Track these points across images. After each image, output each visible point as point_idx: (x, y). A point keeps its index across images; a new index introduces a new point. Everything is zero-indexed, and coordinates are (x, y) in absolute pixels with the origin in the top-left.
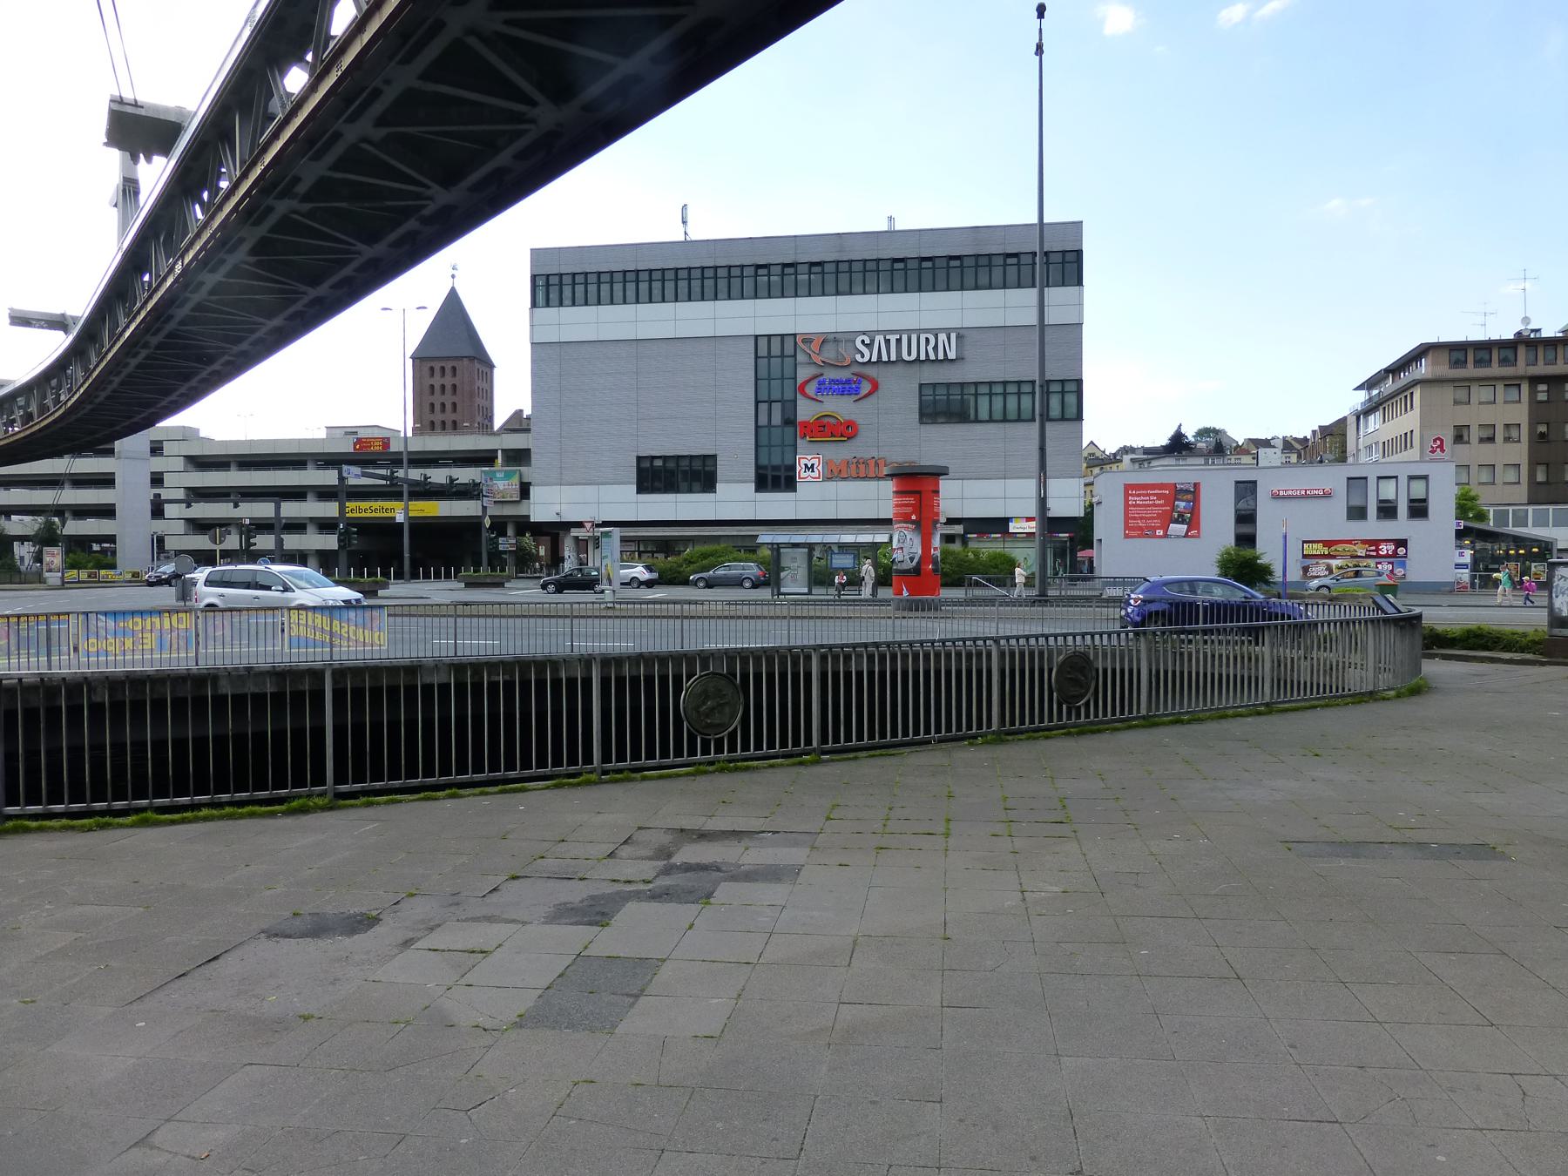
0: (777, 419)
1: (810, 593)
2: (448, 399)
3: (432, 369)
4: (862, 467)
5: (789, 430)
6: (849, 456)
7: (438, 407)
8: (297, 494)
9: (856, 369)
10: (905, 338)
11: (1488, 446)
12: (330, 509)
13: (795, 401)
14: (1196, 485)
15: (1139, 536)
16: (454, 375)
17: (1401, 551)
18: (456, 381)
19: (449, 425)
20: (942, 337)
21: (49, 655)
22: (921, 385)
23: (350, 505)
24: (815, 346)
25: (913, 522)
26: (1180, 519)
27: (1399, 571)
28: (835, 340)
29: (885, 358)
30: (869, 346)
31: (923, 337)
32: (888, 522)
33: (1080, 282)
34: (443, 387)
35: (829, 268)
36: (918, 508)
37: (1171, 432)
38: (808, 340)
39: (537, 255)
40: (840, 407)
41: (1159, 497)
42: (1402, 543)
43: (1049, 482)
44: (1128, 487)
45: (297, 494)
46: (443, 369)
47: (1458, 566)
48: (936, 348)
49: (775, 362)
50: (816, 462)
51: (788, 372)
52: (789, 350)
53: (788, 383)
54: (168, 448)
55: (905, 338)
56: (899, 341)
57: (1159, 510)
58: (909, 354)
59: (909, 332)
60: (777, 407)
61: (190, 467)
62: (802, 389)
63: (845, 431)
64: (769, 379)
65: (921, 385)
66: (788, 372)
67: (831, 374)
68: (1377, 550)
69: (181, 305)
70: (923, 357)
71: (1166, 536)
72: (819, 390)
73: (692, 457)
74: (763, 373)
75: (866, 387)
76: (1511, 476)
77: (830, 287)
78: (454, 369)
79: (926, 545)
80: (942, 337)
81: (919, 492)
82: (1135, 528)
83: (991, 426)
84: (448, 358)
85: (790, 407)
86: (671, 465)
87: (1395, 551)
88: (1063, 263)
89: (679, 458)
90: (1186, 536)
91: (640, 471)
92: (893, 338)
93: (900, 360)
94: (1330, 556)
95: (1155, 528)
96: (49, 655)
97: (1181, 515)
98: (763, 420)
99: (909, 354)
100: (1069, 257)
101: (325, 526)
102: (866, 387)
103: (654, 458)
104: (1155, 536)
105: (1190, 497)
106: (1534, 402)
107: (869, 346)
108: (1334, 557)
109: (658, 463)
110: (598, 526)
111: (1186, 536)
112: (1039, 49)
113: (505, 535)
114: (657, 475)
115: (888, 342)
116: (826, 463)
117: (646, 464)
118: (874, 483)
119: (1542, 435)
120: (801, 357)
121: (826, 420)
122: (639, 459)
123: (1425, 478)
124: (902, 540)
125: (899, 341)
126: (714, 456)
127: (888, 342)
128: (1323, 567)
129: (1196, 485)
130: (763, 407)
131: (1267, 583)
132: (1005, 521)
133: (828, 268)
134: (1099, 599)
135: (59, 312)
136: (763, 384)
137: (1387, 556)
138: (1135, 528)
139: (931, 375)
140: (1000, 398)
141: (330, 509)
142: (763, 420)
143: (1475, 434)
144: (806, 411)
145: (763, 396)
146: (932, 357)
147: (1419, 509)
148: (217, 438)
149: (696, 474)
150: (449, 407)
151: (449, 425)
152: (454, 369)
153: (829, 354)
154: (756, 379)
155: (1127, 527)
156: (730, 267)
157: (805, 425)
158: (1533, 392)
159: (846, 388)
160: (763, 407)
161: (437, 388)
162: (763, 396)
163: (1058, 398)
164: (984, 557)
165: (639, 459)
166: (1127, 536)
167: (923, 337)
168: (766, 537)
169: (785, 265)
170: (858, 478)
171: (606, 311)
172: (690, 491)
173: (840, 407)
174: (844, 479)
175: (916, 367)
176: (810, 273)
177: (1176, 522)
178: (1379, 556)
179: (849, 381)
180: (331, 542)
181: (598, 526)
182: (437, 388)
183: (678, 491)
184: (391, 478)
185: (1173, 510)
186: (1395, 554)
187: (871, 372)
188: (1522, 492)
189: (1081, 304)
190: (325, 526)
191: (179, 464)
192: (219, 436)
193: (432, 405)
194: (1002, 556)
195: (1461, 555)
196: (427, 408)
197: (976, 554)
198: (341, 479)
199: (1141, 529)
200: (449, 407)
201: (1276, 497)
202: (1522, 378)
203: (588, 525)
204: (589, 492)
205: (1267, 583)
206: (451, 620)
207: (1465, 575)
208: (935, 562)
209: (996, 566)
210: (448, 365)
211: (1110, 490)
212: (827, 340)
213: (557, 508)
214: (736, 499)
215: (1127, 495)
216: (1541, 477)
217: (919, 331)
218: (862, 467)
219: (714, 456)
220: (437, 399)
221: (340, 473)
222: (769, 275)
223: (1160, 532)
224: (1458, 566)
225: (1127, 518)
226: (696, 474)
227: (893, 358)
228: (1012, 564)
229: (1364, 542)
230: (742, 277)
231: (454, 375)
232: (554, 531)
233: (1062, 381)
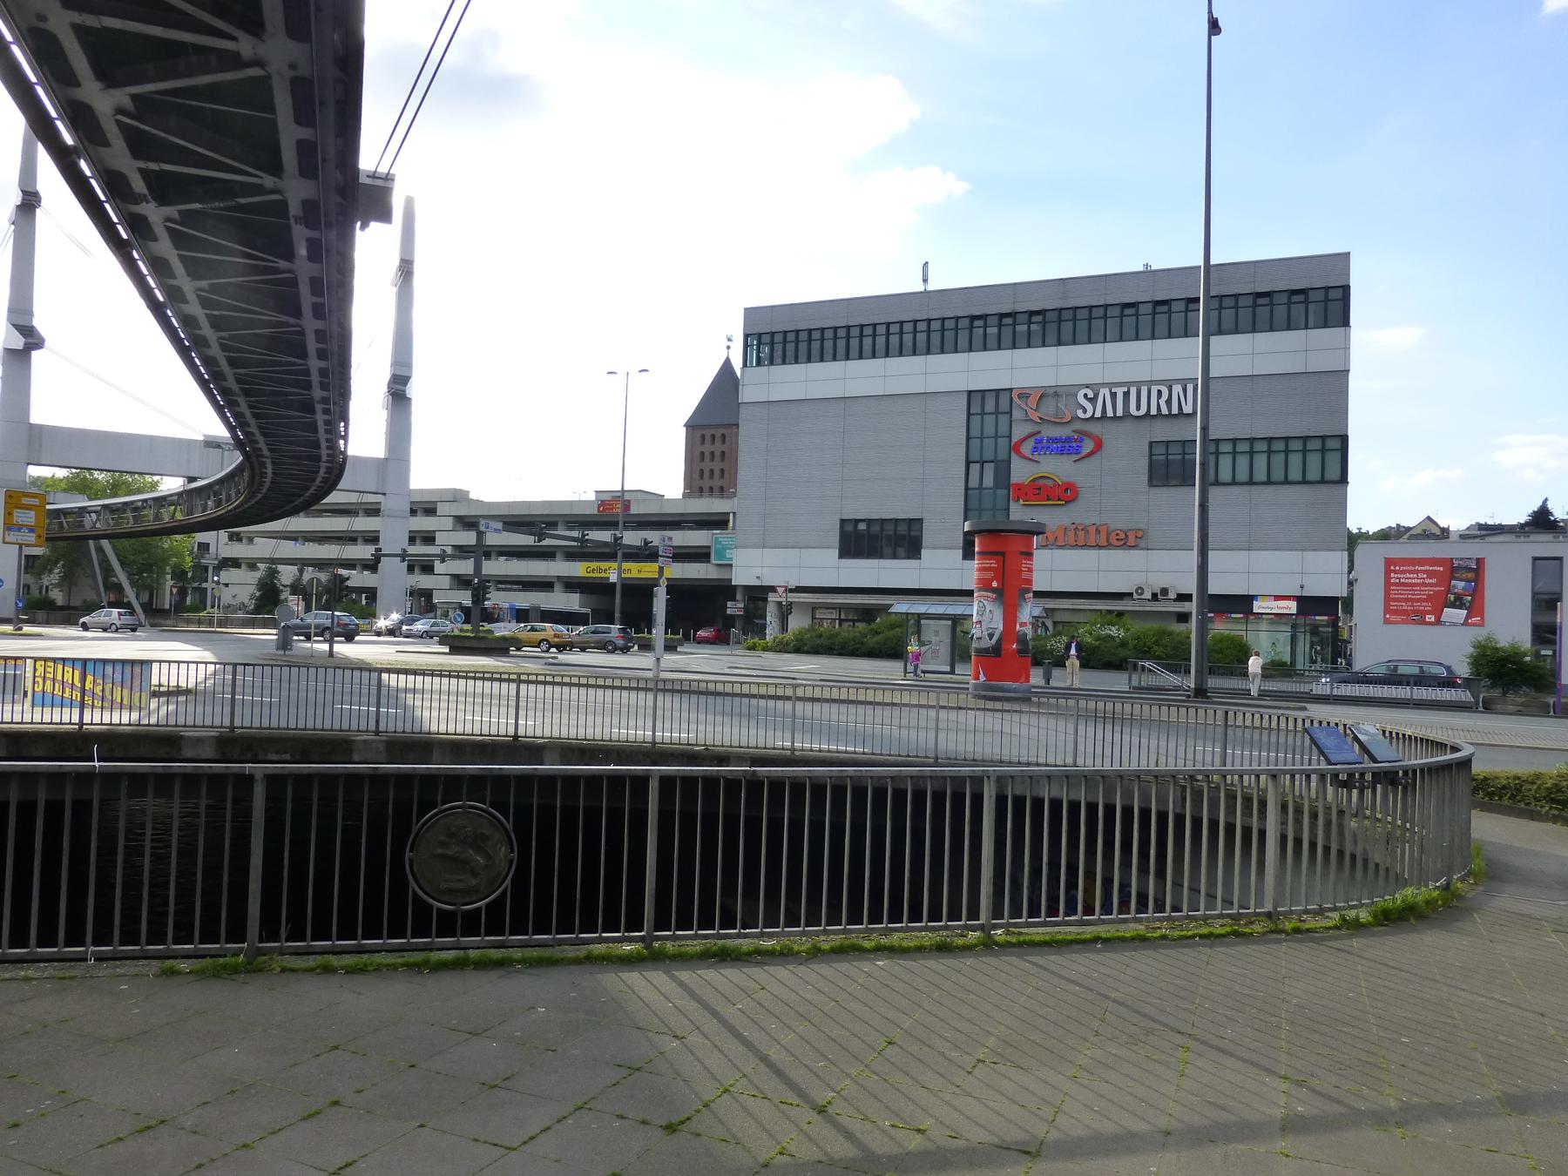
0: (989, 481)
1: (952, 672)
3: (703, 437)
5: (1002, 492)
6: (1067, 522)
7: (707, 473)
8: (544, 585)
9: (1077, 426)
10: (1133, 391)
12: (579, 569)
13: (1009, 461)
14: (1480, 562)
15: (1403, 622)
16: (724, 442)
18: (725, 448)
19: (706, 489)
20: (1177, 389)
21: (233, 700)
22: (1151, 443)
23: (625, 565)
24: (1032, 402)
25: (993, 590)
26: (1458, 603)
28: (1056, 395)
29: (1110, 413)
30: (1093, 400)
31: (1154, 390)
32: (969, 593)
33: (1345, 322)
34: (712, 454)
35: (1052, 316)
36: (1002, 573)
37: (1535, 506)
38: (1024, 396)
39: (750, 313)
40: (1057, 468)
41: (1431, 574)
44: (1389, 562)
45: (544, 585)
46: (713, 436)
48: (1169, 402)
49: (990, 420)
51: (1003, 429)
52: (1004, 406)
53: (1003, 442)
54: (441, 509)
55: (1133, 391)
56: (1126, 394)
57: (1430, 591)
58: (1138, 408)
59: (1139, 384)
60: (989, 468)
61: (459, 527)
62: (1016, 448)
63: (1065, 494)
64: (982, 438)
65: (1151, 443)
66: (1003, 429)
67: (1049, 432)
70: (1154, 411)
71: (1438, 622)
72: (1035, 449)
73: (883, 521)
74: (975, 432)
75: (1088, 446)
77: (1051, 337)
78: (724, 436)
79: (1010, 617)
80: (1177, 389)
81: (1003, 554)
82: (1399, 610)
83: (1235, 490)
84: (718, 426)
85: (1003, 469)
86: (876, 528)
88: (1327, 300)
89: (883, 521)
90: (1465, 623)
91: (844, 536)
92: (1120, 392)
93: (1127, 415)
95: (1425, 613)
96: (233, 700)
97: (1459, 597)
98: (974, 482)
99: (1138, 408)
100: (1333, 294)
101: (571, 585)
102: (1088, 446)
103: (857, 521)
104: (1425, 623)
105: (1470, 575)
107: (1093, 400)
109: (862, 526)
110: (791, 591)
111: (1465, 623)
112: (1214, 27)
113: (734, 599)
114: (860, 540)
115: (1114, 395)
117: (849, 528)
118: (1093, 553)
120: (1017, 414)
121: (1042, 482)
122: (843, 522)
124: (981, 613)
125: (1126, 394)
126: (920, 521)
127: (1114, 395)
129: (1480, 562)
133: (1050, 316)
136: (975, 443)
138: (1399, 610)
139: (1163, 431)
140: (1264, 457)
141: (579, 569)
142: (974, 482)
144: (1021, 472)
145: (975, 456)
146: (1165, 411)
148: (487, 499)
149: (903, 539)
150: (717, 473)
151: (706, 489)
152: (724, 436)
153: (1048, 409)
154: (968, 438)
155: (1387, 610)
156: (944, 319)
157: (1019, 487)
159: (1066, 446)
160: (975, 468)
163: (1322, 457)
165: (843, 522)
166: (1386, 621)
167: (1154, 390)
168: (901, 606)
169: (1002, 316)
171: (816, 369)
172: (895, 556)
173: (1057, 468)
174: (1061, 547)
175: (1146, 423)
176: (1030, 323)
177: (1453, 605)
179: (1069, 440)
181: (791, 591)
183: (881, 557)
184: (541, 537)
185: (1448, 591)
187: (1095, 429)
189: (1347, 348)
190: (571, 585)
191: (448, 523)
192: (487, 498)
193: (702, 471)
194: (1230, 639)
196: (696, 475)
199: (1405, 612)
200: (717, 473)
203: (780, 590)
204: (791, 555)
206: (513, 686)
208: (1022, 639)
209: (1220, 651)
210: (708, 433)
211: (1370, 562)
212: (1044, 395)
213: (758, 572)
215: (1388, 572)
217: (1150, 383)
219: (920, 521)
220: (707, 465)
222: (985, 326)
223: (1431, 618)
225: (1388, 599)
226: (903, 539)
227: (1120, 413)
228: (1244, 653)
230: (957, 329)
231: (724, 442)
232: (757, 595)
233: (1323, 438)
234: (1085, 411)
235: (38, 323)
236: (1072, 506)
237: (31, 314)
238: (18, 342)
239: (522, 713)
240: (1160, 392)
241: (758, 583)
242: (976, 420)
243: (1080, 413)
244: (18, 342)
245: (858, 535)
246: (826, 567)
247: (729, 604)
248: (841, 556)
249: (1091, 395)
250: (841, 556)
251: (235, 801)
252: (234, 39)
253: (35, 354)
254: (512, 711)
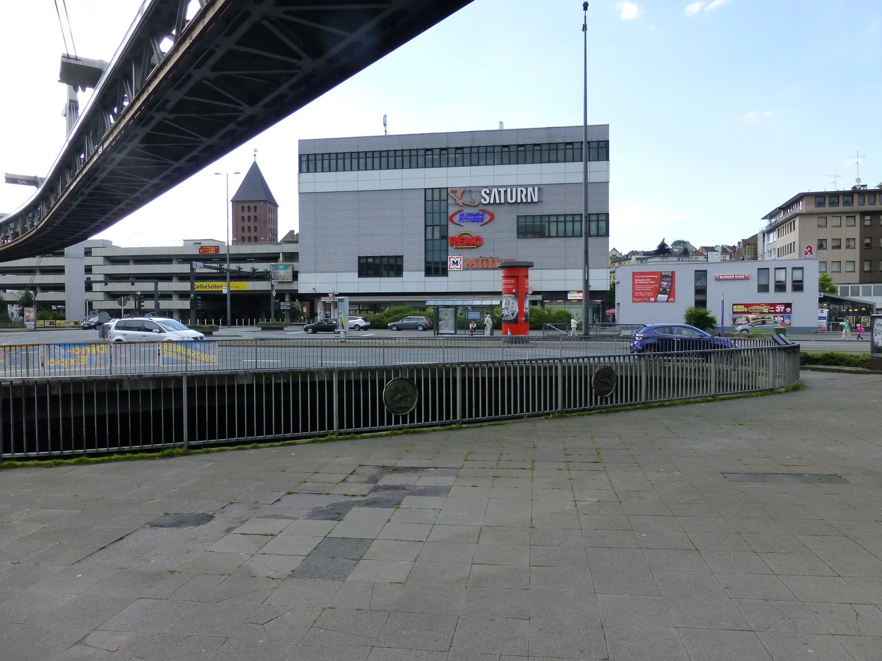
0: (437, 235)
1: (455, 333)
2: (252, 224)
3: (243, 207)
4: (485, 262)
5: (444, 242)
6: (478, 257)
7: (246, 229)
8: (167, 277)
9: (481, 207)
10: (509, 190)
11: (837, 251)
12: (185, 286)
13: (447, 225)
14: (673, 273)
15: (641, 302)
16: (256, 211)
17: (788, 310)
18: (257, 214)
19: (253, 239)
20: (530, 189)
21: (28, 368)
22: (518, 217)
23: (197, 284)
24: (458, 195)
25: (513, 293)
26: (664, 292)
27: (787, 321)
28: (470, 191)
29: (498, 201)
30: (489, 194)
31: (519, 190)
32: (499, 293)
33: (607, 159)
34: (249, 217)
35: (466, 151)
36: (517, 286)
37: (659, 243)
38: (454, 191)
39: (302, 143)
40: (472, 229)
41: (652, 279)
42: (789, 305)
43: (590, 271)
44: (634, 274)
45: (167, 277)
46: (249, 207)
47: (820, 318)
48: (526, 195)
49: (436, 203)
50: (459, 259)
51: (443, 209)
52: (444, 197)
53: (443, 216)
54: (94, 252)
55: (509, 190)
56: (506, 192)
57: (652, 287)
58: (512, 199)
59: (511, 186)
60: (437, 229)
61: (107, 263)
62: (451, 218)
63: (475, 242)
64: (433, 213)
65: (518, 217)
66: (443, 209)
67: (467, 210)
68: (775, 309)
69: (102, 172)
70: (519, 201)
71: (656, 301)
72: (461, 219)
73: (389, 257)
74: (429, 210)
75: (487, 218)
76: (850, 267)
77: (467, 161)
78: (255, 207)
79: (521, 306)
80: (530, 189)
81: (517, 277)
82: (638, 297)
83: (558, 239)
84: (252, 201)
85: (444, 229)
86: (377, 261)
87: (785, 310)
88: (598, 148)
89: (382, 257)
90: (667, 301)
91: (360, 265)
92: (502, 190)
93: (506, 202)
94: (748, 313)
95: (650, 297)
96: (28, 368)
97: (664, 289)
98: (429, 236)
99: (512, 199)
100: (601, 145)
101: (183, 295)
102: (487, 218)
103: (368, 257)
104: (650, 301)
105: (669, 279)
106: (863, 226)
107: (489, 194)
108: (750, 313)
109: (370, 260)
110: (337, 295)
111: (667, 301)
113: (284, 301)
114: (369, 267)
115: (499, 192)
116: (465, 260)
117: (364, 261)
118: (491, 272)
119: (867, 245)
120: (450, 201)
121: (464, 236)
122: (360, 258)
123: (802, 268)
124: (507, 304)
125: (506, 192)
126: (402, 257)
127: (499, 192)
128: (744, 319)
129: (673, 273)
130: (429, 229)
131: (713, 327)
132: (565, 293)
133: (466, 151)
134: (618, 336)
135: (33, 175)
136: (429, 216)
137: (780, 312)
138: (638, 297)
139: (523, 211)
140: (563, 224)
141: (185, 286)
142: (429, 236)
143: (830, 244)
144: (453, 231)
145: (429, 222)
146: (524, 200)
147: (798, 286)
148: (122, 246)
149: (392, 266)
150: (252, 229)
151: (253, 239)
152: (255, 207)
153: (466, 199)
154: (426, 213)
155: (634, 296)
156: (411, 150)
157: (453, 239)
158: (862, 221)
159: (476, 218)
160: (429, 229)
161: (246, 218)
162: (429, 222)
163: (595, 224)
164: (553, 313)
165: (360, 258)
166: (634, 301)
167: (519, 190)
168: (431, 302)
169: (441, 149)
170: (483, 269)
171: (341, 175)
172: (388, 276)
173: (472, 229)
174: (475, 269)
175: (515, 206)
176: (456, 154)
177: (662, 293)
178: (776, 313)
179: (477, 214)
180: (186, 305)
181: (337, 295)
182: (246, 218)
183: (381, 276)
184: (220, 269)
185: (660, 286)
186: (785, 312)
187: (490, 209)
188: (856, 276)
189: (608, 171)
190: (183, 295)
191: (101, 261)
192: (123, 245)
193: (243, 228)
194: (563, 312)
195: (822, 312)
196: (240, 230)
197: (549, 312)
198: (192, 269)
199: (642, 297)
200: (252, 229)
201: (718, 279)
202: (856, 212)
203: (331, 295)
204: (332, 276)
205: (713, 327)
206: (254, 349)
207: (824, 323)
208: (526, 316)
209: (560, 318)
210: (252, 205)
211: (624, 275)
212: (465, 191)
213: (313, 286)
214: (414, 280)
215: (634, 278)
216: (867, 268)
217: (517, 186)
218: (485, 262)
219: (402, 257)
220: (246, 224)
221: (191, 266)
222: (433, 155)
223: (652, 299)
224: (820, 318)
225: (634, 291)
226: (392, 266)
227: (502, 201)
228: (569, 317)
229: (767, 305)
230: (417, 155)
231: (256, 211)
232: (311, 299)
233: (598, 214)
239: (31, 365)
251: (27, 423)
252: (285, 13)
254: (24, 365)
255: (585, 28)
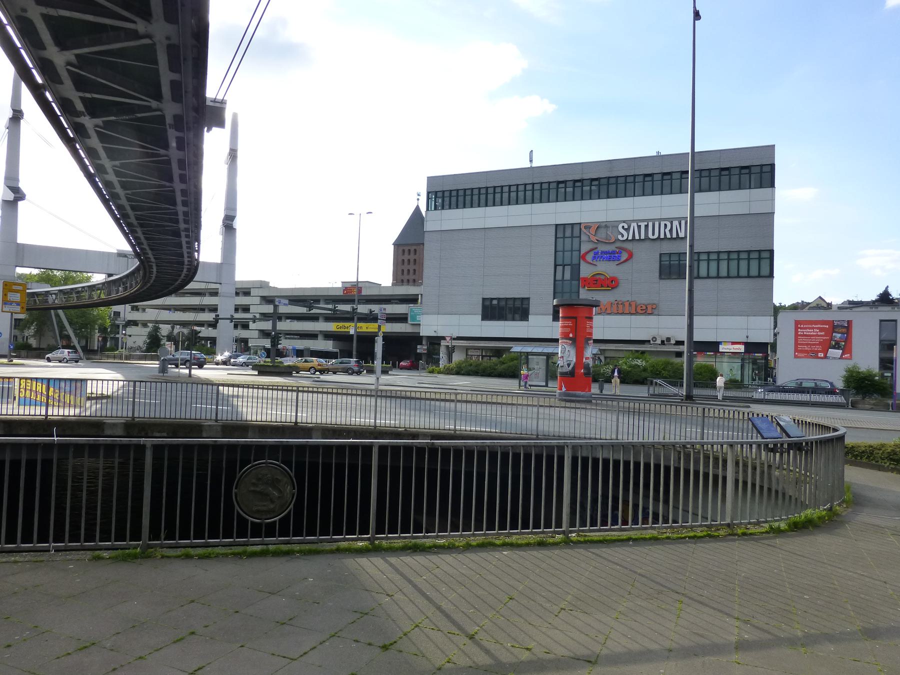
0: (567, 276)
1: (547, 386)
3: (404, 251)
5: (575, 283)
6: (612, 300)
7: (406, 272)
9: (618, 244)
10: (650, 225)
12: (332, 327)
13: (579, 264)
14: (850, 322)
15: (805, 357)
16: (415, 254)
18: (416, 257)
19: (405, 281)
20: (676, 223)
21: (134, 402)
22: (661, 254)
23: (359, 325)
24: (593, 231)
25: (570, 339)
26: (837, 346)
28: (606, 227)
29: (637, 237)
30: (627, 230)
31: (662, 224)
32: (556, 341)
33: (772, 185)
34: (409, 260)
35: (604, 182)
36: (575, 329)
37: (881, 290)
38: (588, 227)
39: (431, 180)
40: (607, 268)
41: (821, 330)
44: (797, 323)
46: (409, 250)
48: (671, 231)
49: (568, 241)
51: (576, 246)
52: (576, 233)
53: (575, 254)
54: (253, 292)
55: (650, 225)
56: (647, 226)
57: (821, 339)
58: (653, 234)
59: (654, 221)
60: (568, 269)
61: (263, 302)
62: (583, 257)
63: (612, 283)
64: (564, 251)
65: (661, 254)
66: (576, 246)
67: (602, 248)
70: (662, 236)
71: (825, 357)
72: (594, 258)
73: (507, 299)
74: (560, 248)
75: (625, 256)
77: (603, 193)
78: (415, 250)
79: (580, 354)
80: (676, 223)
81: (576, 318)
82: (803, 350)
83: (709, 281)
84: (412, 245)
85: (576, 269)
86: (503, 303)
88: (761, 172)
89: (507, 299)
90: (841, 358)
91: (484, 308)
92: (643, 225)
93: (647, 238)
95: (818, 352)
96: (134, 402)
97: (837, 343)
98: (559, 277)
99: (653, 234)
100: (765, 169)
101: (328, 336)
102: (625, 256)
103: (492, 299)
104: (818, 357)
105: (844, 330)
107: (627, 230)
109: (495, 302)
110: (454, 339)
111: (841, 358)
113: (421, 344)
114: (494, 310)
115: (639, 227)
117: (488, 303)
118: (628, 317)
120: (584, 238)
121: (598, 277)
122: (484, 299)
124: (563, 352)
125: (647, 226)
126: (528, 299)
127: (639, 227)
129: (850, 322)
133: (603, 181)
135: (391, 249)
136: (560, 254)
138: (803, 350)
139: (668, 248)
140: (726, 262)
141: (332, 327)
142: (559, 277)
144: (586, 271)
145: (559, 262)
146: (668, 236)
148: (279, 287)
149: (518, 309)
150: (412, 271)
151: (405, 281)
152: (415, 250)
153: (602, 235)
154: (556, 252)
155: (796, 350)
156: (542, 183)
157: (585, 279)
159: (612, 256)
160: (560, 268)
163: (759, 262)
165: (484, 299)
166: (796, 357)
167: (662, 224)
168: (517, 348)
169: (575, 181)
171: (468, 212)
172: (513, 319)
173: (607, 268)
174: (609, 314)
175: (658, 243)
176: (591, 185)
177: (834, 348)
179: (613, 252)
181: (454, 339)
183: (506, 320)
184: (311, 308)
185: (831, 339)
187: (629, 246)
189: (773, 200)
190: (328, 336)
191: (257, 300)
192: (280, 286)
193: (403, 271)
194: (706, 367)
196: (400, 273)
199: (806, 352)
200: (412, 271)
203: (448, 339)
204: (454, 319)
206: (295, 394)
208: (587, 367)
209: (701, 374)
210: (406, 249)
211: (787, 323)
212: (599, 227)
213: (435, 328)
215: (796, 328)
217: (660, 220)
219: (528, 299)
220: (406, 267)
222: (566, 187)
223: (821, 355)
225: (796, 344)
226: (518, 309)
227: (643, 237)
228: (714, 375)
230: (549, 189)
231: (415, 254)
232: (435, 341)
233: (759, 251)
234: (623, 236)
235: (22, 185)
236: (615, 291)
237: (18, 180)
238: (11, 196)
240: (666, 225)
241: (435, 335)
242: (560, 241)
243: (620, 237)
244: (11, 196)
245: (492, 307)
246: (474, 325)
247: (419, 347)
248: (483, 319)
249: (626, 227)
250: (483, 319)
251: (135, 460)
253: (20, 203)
255: (697, 15)
